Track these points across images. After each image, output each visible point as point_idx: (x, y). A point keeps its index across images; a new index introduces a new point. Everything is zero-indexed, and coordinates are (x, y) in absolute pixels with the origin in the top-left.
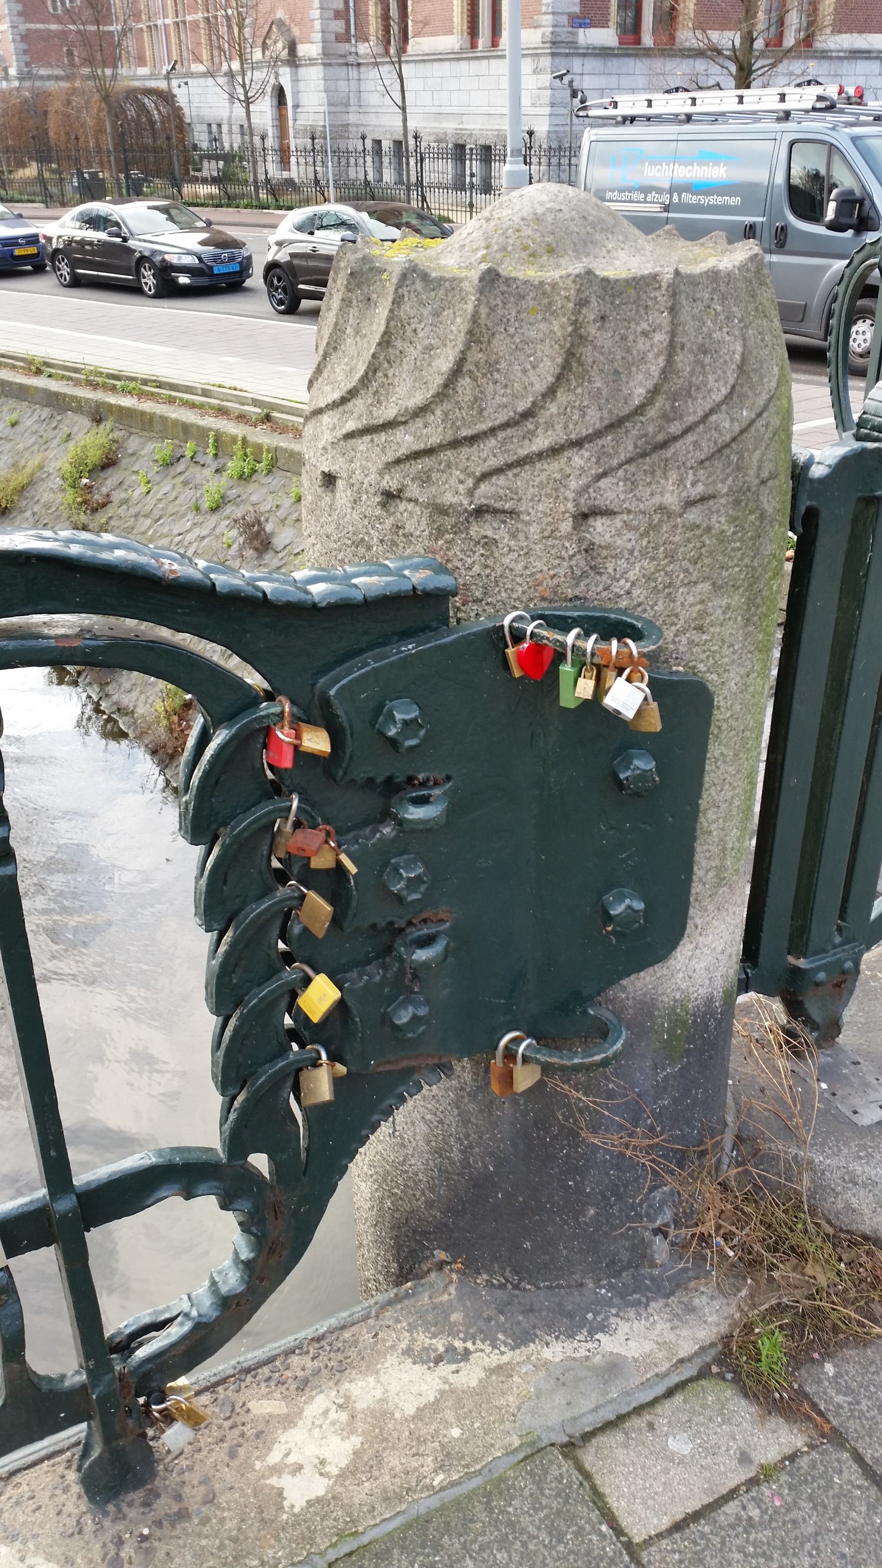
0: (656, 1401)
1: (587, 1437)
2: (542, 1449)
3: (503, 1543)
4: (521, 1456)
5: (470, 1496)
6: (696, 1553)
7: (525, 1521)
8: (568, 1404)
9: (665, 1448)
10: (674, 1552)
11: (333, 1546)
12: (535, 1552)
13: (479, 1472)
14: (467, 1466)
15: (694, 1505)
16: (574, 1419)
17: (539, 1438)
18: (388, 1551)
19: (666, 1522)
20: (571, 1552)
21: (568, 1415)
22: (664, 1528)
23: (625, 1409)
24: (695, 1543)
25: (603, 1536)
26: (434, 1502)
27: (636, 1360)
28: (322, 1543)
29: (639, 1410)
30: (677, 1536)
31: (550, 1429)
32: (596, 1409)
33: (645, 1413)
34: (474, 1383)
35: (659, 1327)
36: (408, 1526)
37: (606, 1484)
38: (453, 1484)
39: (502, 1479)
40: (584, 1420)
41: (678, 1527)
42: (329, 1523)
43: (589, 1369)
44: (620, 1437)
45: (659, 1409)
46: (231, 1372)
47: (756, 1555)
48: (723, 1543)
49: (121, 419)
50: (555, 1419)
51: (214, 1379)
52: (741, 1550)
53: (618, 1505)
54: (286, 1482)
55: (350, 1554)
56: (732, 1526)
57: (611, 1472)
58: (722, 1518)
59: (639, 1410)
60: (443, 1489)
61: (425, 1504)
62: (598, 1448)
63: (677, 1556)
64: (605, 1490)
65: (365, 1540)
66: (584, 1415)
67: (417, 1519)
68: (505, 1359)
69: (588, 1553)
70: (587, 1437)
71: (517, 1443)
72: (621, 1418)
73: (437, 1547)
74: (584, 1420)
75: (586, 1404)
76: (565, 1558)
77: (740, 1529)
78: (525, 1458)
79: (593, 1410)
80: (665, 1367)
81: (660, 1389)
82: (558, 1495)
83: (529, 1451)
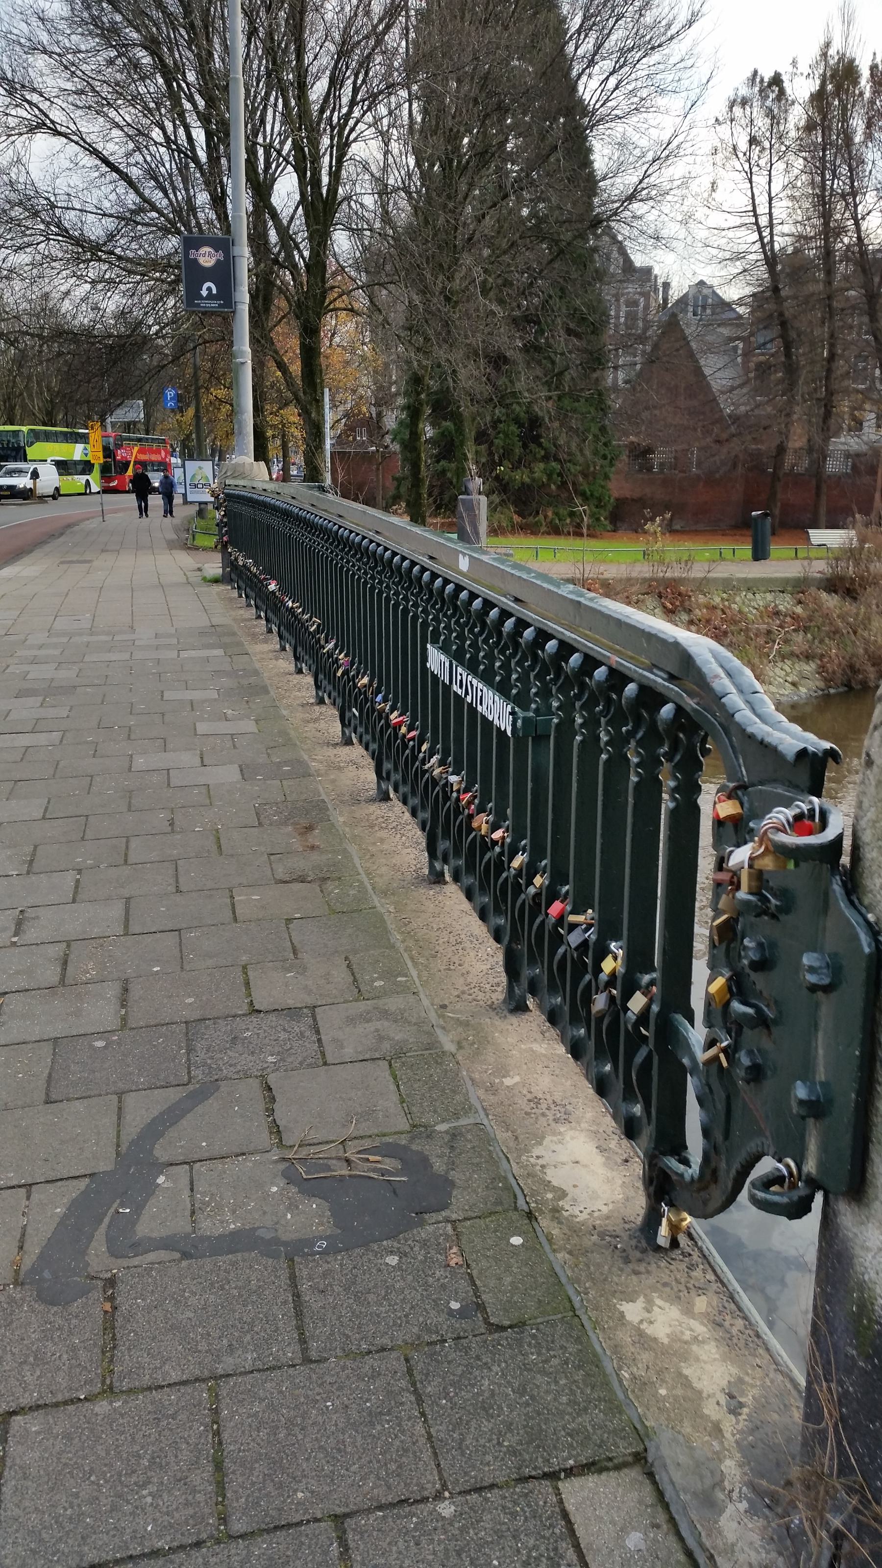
0: (681, 1539)
1: (651, 1475)
2: (643, 1442)
3: (572, 1403)
4: (638, 1426)
5: (611, 1391)
6: (541, 1516)
7: (587, 1418)
8: (678, 1464)
9: (634, 1529)
10: (545, 1503)
11: (590, 1318)
12: (563, 1419)
13: (627, 1397)
14: (633, 1391)
15: (580, 1532)
16: (665, 1466)
17: (650, 1440)
18: (581, 1343)
19: (570, 1508)
20: (558, 1439)
21: (668, 1461)
22: (566, 1505)
23: (673, 1509)
24: (549, 1518)
25: (566, 1459)
26: (609, 1369)
27: (716, 1522)
28: (593, 1314)
29: (672, 1520)
30: (557, 1509)
31: (658, 1448)
32: (672, 1483)
33: (670, 1526)
34: (706, 1411)
35: (753, 1554)
36: (595, 1354)
37: (610, 1479)
38: (620, 1381)
39: (621, 1412)
40: (664, 1474)
41: (565, 1515)
42: (606, 1318)
43: (714, 1487)
44: (649, 1500)
45: (672, 1539)
46: (731, 1288)
47: (529, 1556)
48: (544, 1537)
49: (434, 132)
50: (665, 1451)
51: (725, 1281)
52: (535, 1547)
53: (591, 1481)
54: (640, 1303)
55: (583, 1326)
56: (556, 1549)
57: (619, 1485)
58: (564, 1545)
59: (672, 1520)
60: (618, 1375)
61: (609, 1367)
62: (641, 1483)
63: (541, 1503)
64: (604, 1476)
65: (590, 1333)
66: (668, 1473)
67: (599, 1360)
68: (728, 1435)
69: (555, 1447)
70: (651, 1475)
71: (647, 1424)
72: (666, 1507)
73: (579, 1367)
74: (664, 1474)
75: (677, 1476)
76: (555, 1434)
77: (552, 1554)
78: (635, 1428)
79: (671, 1480)
80: (708, 1543)
81: (691, 1543)
82: (602, 1441)
83: (642, 1432)
